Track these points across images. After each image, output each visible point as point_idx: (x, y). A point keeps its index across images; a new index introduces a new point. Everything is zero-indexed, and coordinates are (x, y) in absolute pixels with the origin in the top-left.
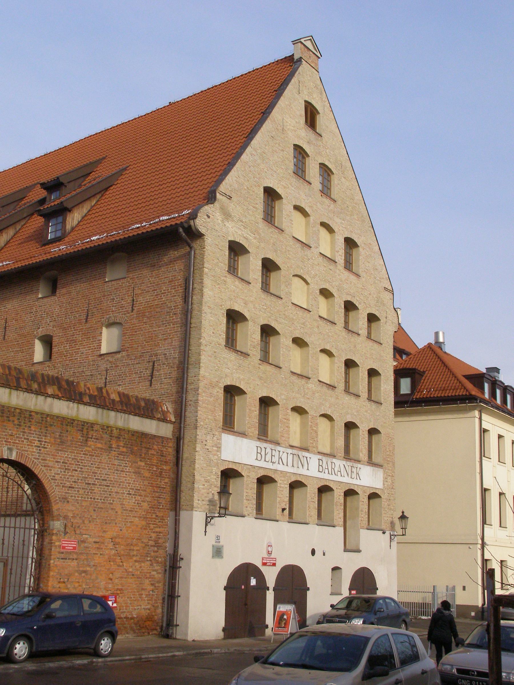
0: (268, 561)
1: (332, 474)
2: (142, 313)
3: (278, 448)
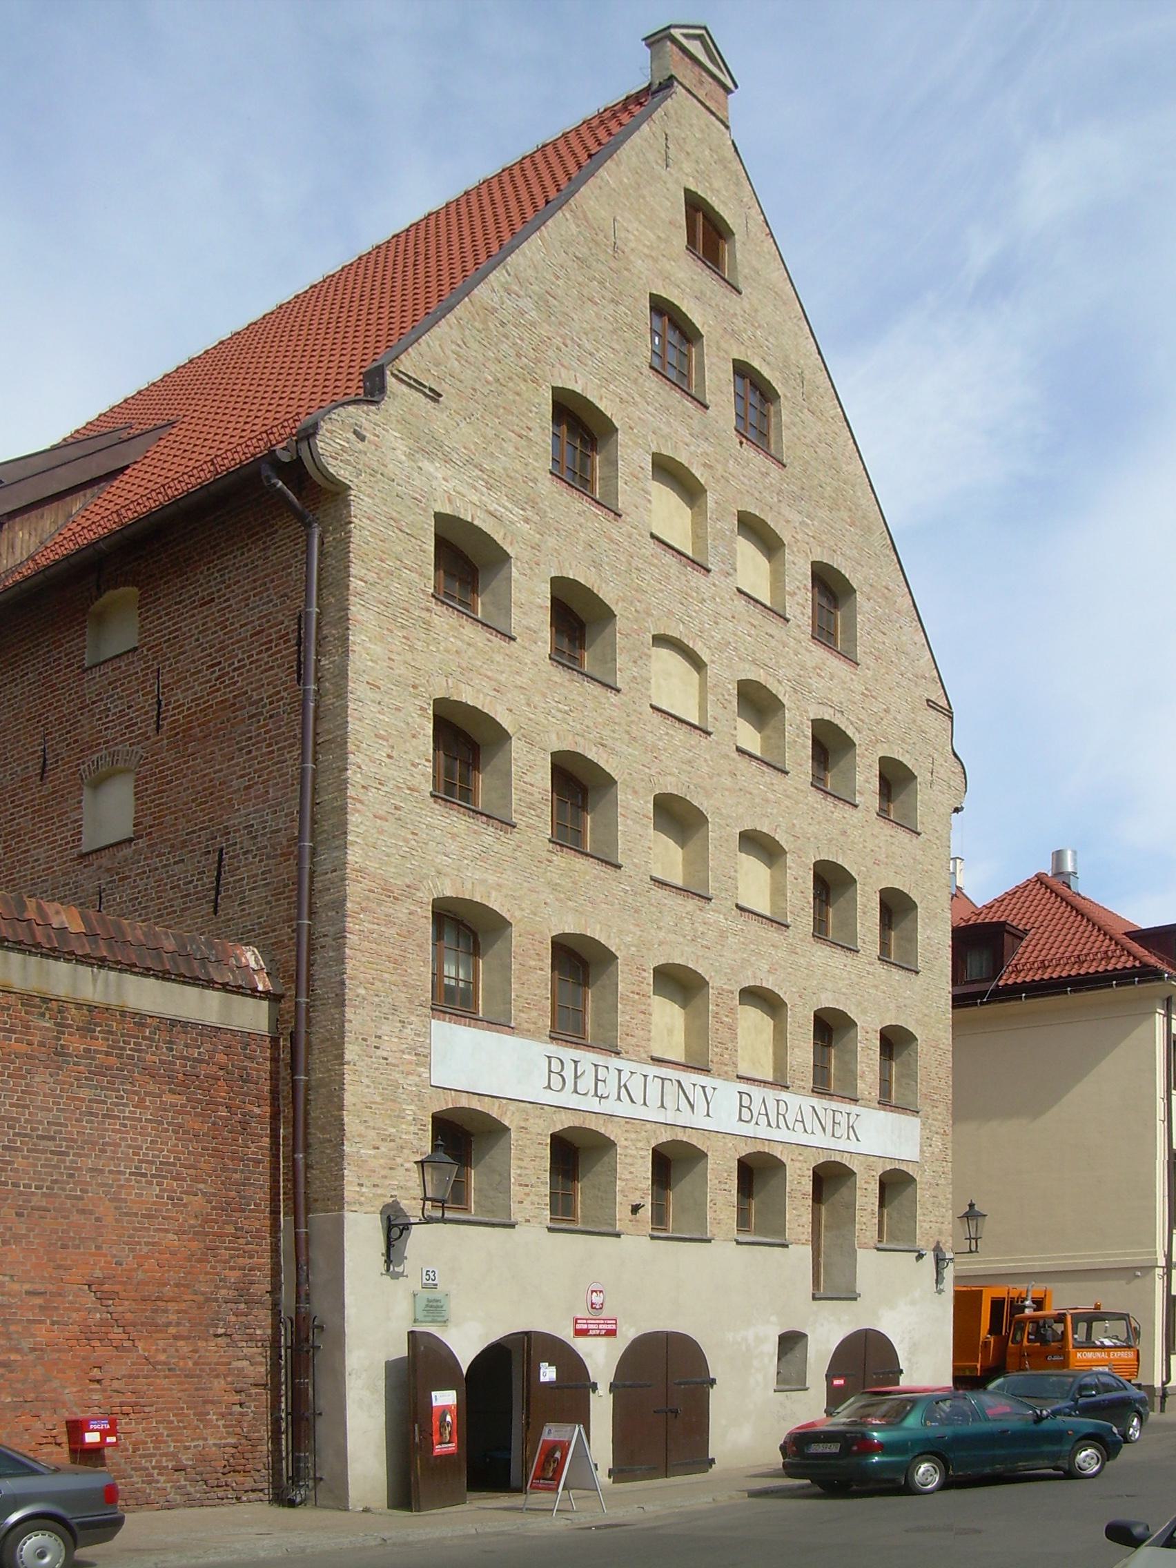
0: (591, 1327)
1: (778, 1126)
2: (184, 731)
3: (614, 1062)
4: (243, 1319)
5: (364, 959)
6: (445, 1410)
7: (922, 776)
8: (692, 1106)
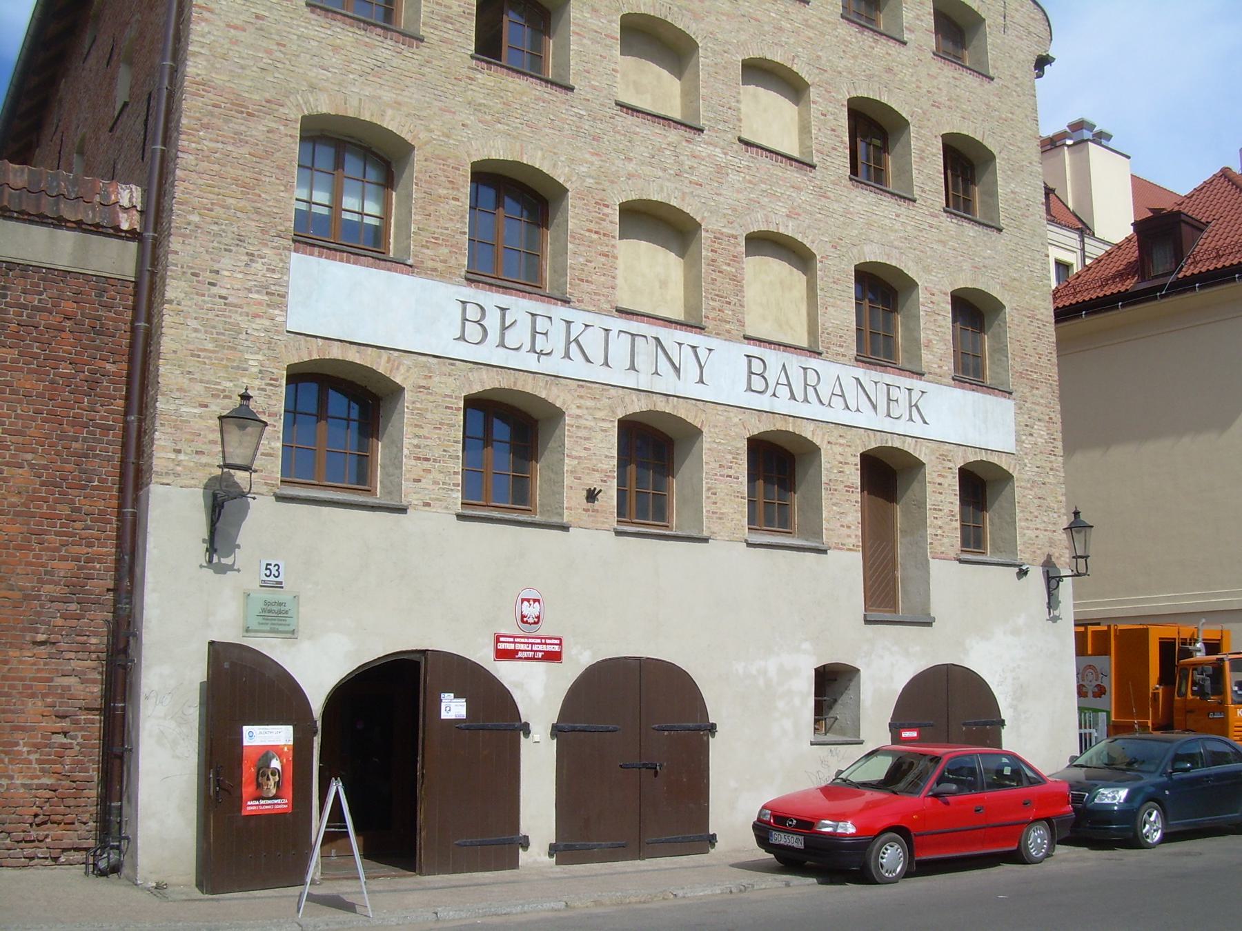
0: (519, 647)
1: (806, 400)
4: (74, 623)
5: (200, 182)
6: (266, 754)
7: (992, 19)
8: (677, 370)
